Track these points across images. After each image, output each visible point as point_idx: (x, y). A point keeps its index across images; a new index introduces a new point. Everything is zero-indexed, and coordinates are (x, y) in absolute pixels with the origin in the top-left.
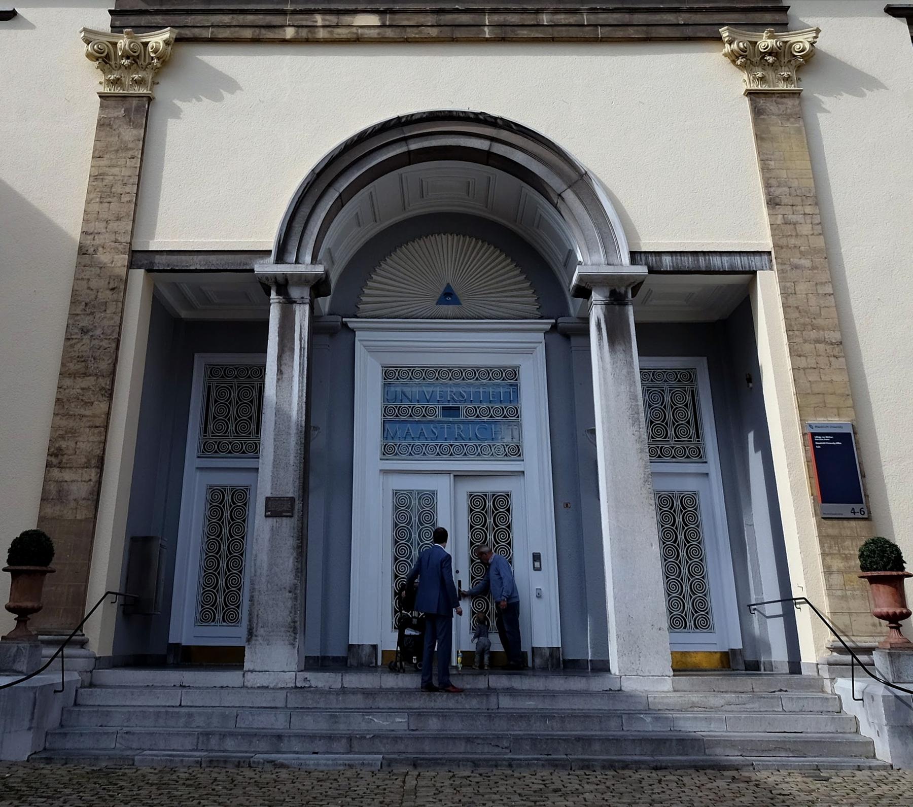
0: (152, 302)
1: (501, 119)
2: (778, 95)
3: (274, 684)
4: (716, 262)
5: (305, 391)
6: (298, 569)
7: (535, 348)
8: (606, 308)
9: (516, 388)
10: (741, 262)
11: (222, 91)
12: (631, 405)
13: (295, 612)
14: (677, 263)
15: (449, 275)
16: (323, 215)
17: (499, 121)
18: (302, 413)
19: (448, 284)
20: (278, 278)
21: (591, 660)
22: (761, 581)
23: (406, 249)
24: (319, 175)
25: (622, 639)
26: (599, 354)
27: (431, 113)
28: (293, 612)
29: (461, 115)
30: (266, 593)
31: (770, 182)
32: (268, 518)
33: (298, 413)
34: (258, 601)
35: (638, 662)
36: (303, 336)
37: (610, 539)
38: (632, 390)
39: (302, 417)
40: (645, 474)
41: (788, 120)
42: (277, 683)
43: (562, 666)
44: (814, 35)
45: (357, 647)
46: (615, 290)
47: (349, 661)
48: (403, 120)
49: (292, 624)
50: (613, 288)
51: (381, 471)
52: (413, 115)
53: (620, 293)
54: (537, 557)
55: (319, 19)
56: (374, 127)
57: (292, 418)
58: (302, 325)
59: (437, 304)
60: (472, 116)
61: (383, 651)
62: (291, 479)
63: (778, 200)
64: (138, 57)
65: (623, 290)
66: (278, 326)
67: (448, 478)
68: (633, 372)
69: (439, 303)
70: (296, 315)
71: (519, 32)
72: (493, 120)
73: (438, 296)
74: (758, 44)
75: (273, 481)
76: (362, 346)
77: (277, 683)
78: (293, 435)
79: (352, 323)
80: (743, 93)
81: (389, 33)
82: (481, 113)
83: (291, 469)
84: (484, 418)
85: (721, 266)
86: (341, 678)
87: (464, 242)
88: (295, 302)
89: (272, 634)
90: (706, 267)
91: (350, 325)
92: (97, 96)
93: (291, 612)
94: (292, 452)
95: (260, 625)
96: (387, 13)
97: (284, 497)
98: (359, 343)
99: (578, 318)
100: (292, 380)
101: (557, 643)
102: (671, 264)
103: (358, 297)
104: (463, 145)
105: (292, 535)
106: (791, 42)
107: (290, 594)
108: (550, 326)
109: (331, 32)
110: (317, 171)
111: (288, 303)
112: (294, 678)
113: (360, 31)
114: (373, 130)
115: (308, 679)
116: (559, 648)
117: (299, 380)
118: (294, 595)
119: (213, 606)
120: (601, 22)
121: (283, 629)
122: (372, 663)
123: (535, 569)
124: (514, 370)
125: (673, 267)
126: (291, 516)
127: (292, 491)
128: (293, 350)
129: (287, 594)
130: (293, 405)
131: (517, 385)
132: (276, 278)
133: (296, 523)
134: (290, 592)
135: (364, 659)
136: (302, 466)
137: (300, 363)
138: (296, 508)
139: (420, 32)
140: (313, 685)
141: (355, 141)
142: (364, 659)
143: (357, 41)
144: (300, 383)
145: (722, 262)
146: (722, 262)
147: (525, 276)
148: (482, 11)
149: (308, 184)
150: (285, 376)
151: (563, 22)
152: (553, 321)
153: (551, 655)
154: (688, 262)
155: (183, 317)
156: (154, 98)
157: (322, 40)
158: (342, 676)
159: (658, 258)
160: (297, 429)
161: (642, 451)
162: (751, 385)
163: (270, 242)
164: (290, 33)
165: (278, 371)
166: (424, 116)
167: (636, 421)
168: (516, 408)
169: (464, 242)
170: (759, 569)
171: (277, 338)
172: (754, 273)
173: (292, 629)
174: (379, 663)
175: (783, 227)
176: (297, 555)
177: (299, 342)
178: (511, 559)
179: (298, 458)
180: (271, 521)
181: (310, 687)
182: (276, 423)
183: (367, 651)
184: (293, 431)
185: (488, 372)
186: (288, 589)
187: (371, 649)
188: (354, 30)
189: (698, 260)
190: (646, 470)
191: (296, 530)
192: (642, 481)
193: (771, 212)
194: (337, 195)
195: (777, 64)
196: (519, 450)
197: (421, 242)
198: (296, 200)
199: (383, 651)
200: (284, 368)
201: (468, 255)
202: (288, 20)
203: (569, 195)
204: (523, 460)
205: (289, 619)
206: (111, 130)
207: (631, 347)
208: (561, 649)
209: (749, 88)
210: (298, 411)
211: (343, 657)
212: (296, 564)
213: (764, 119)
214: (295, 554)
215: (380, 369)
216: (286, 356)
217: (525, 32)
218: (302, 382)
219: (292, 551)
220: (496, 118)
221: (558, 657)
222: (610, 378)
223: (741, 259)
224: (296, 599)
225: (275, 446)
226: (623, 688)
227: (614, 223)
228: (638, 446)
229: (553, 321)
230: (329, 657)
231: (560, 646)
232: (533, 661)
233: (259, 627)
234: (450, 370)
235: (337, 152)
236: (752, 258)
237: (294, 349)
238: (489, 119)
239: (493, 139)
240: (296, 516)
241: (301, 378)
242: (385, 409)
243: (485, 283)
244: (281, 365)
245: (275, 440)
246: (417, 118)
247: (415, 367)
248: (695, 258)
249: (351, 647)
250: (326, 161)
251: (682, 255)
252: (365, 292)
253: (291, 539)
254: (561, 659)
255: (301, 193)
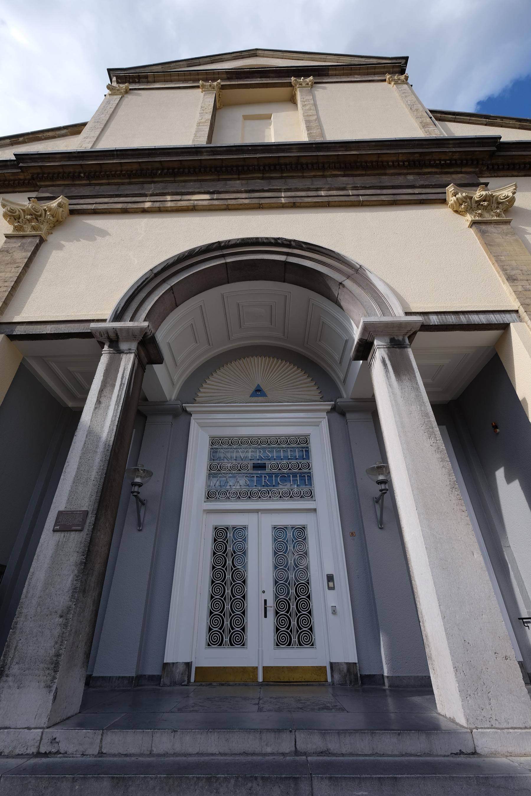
0: (18, 369)
1: (295, 241)
2: (495, 224)
3: (10, 749)
4: (475, 319)
5: (118, 416)
6: (75, 589)
7: (321, 422)
8: (388, 350)
9: (307, 452)
10: (495, 318)
11: (96, 236)
12: (425, 421)
13: (62, 642)
14: (442, 320)
15: (259, 380)
16: (156, 299)
17: (292, 243)
18: (111, 434)
19: (258, 385)
20: (109, 332)
21: (388, 677)
22: (528, 596)
23: (231, 365)
24: (157, 275)
25: (462, 673)
26: (388, 383)
27: (243, 239)
28: (59, 642)
29: (265, 241)
30: (33, 619)
31: (504, 267)
32: (55, 533)
33: (108, 435)
34: (21, 629)
35: (488, 707)
36: (125, 375)
37: (426, 548)
38: (423, 409)
39: (111, 438)
40: (450, 481)
41: (506, 235)
42: (15, 748)
43: (360, 682)
44: (514, 188)
45: (171, 665)
46: (394, 338)
47: (162, 680)
48: (222, 244)
49: (55, 659)
50: (392, 337)
51: (204, 511)
52: (229, 241)
53: (398, 340)
54: (330, 578)
55: (169, 198)
56: (201, 247)
57: (102, 439)
58: (126, 367)
59: (250, 397)
60: (273, 241)
61: (196, 668)
62: (89, 493)
63: (514, 278)
64: (41, 216)
65: (401, 338)
66: (105, 369)
67: (257, 515)
68: (421, 395)
69: (252, 396)
70: (122, 361)
71: (305, 200)
72: (288, 243)
73: (251, 392)
74: (474, 197)
75: (70, 495)
76: (196, 423)
77: (15, 748)
78: (99, 453)
79: (190, 408)
80: (467, 227)
81: (216, 202)
82: (279, 238)
83: (91, 483)
84: (284, 470)
85: (479, 321)
86: (100, 737)
87: (269, 361)
88: (123, 353)
89: (27, 672)
90: (468, 322)
91: (188, 409)
92: (4, 236)
93: (56, 643)
94: (95, 468)
95: (16, 660)
96: (215, 193)
97: (77, 511)
98: (194, 421)
99: (352, 399)
100: (108, 409)
101: (354, 659)
102: (438, 321)
103: (196, 394)
104: (267, 258)
105: (77, 550)
106: (498, 195)
107: (61, 620)
108: (330, 407)
109: (176, 204)
110: (155, 271)
111: (117, 351)
112: (39, 738)
113: (196, 202)
114: (199, 251)
115: (57, 740)
116: (356, 663)
117: (115, 408)
118: (64, 621)
119: (221, 612)
120: (361, 193)
121: (42, 666)
122: (184, 681)
123: (330, 588)
124: (306, 438)
125: (440, 322)
126: (80, 531)
127: (87, 504)
128: (113, 386)
129: (57, 619)
130: (105, 428)
131: (307, 447)
132: (107, 333)
133: (85, 536)
134: (61, 616)
135: (177, 677)
136: (102, 480)
137: (118, 395)
138: (88, 521)
139: (237, 201)
140: (62, 751)
141: (186, 257)
142: (177, 677)
143: (193, 209)
144: (115, 410)
145: (479, 319)
146: (479, 319)
147: (311, 379)
148: (280, 191)
149: (146, 279)
150: (103, 405)
151: (335, 194)
152: (333, 403)
153: (348, 670)
154: (451, 320)
155: (70, 406)
156: (46, 240)
157: (170, 209)
158: (102, 735)
159: (426, 317)
160: (105, 448)
161: (443, 460)
162: (498, 430)
163: (107, 312)
164: (148, 205)
165: (97, 401)
166: (238, 242)
167: (431, 435)
168: (308, 463)
169: (269, 361)
170: (524, 584)
171: (102, 378)
172: (505, 327)
173: (53, 665)
174: (192, 679)
175: (525, 293)
176: (79, 572)
177: (120, 380)
178: (308, 580)
179: (100, 473)
180: (59, 536)
181: (58, 752)
182: (85, 444)
183: (181, 668)
184: (100, 449)
185: (288, 440)
186: (59, 612)
187: (185, 667)
188: (192, 202)
189: (460, 318)
190: (451, 478)
191: (82, 545)
192: (449, 488)
193: (512, 284)
194: (169, 287)
195: (489, 207)
196: (311, 493)
197: (241, 362)
198: (136, 287)
199: (196, 668)
200: (103, 400)
201: (272, 367)
202: (148, 199)
203: (348, 283)
204: (315, 500)
205: (52, 652)
206: (7, 254)
207: (415, 377)
208: (358, 665)
209: (473, 219)
210: (108, 432)
211: (158, 675)
212: (75, 582)
213: (488, 235)
214: (76, 572)
215: (208, 439)
216: (106, 392)
217: (310, 200)
218: (117, 410)
219: (73, 567)
220: (290, 241)
221: (355, 672)
222: (400, 400)
223: (494, 316)
224: (65, 625)
225: (80, 463)
226: (479, 751)
227: (387, 296)
228: (438, 456)
229: (333, 403)
230: (145, 675)
231: (357, 662)
232: (332, 676)
233: (14, 663)
234: (259, 439)
235: (171, 261)
236: (504, 315)
237: (115, 385)
238: (285, 242)
239: (288, 254)
240: (86, 530)
241: (116, 407)
242: (210, 466)
243: (284, 383)
244: (101, 397)
245: (81, 458)
246: (232, 243)
247: (234, 437)
248: (457, 316)
249: (165, 665)
250: (162, 266)
251: (446, 314)
252: (201, 391)
253: (76, 554)
254: (359, 675)
255: (140, 283)
